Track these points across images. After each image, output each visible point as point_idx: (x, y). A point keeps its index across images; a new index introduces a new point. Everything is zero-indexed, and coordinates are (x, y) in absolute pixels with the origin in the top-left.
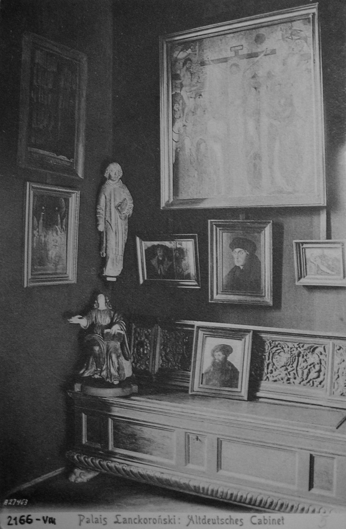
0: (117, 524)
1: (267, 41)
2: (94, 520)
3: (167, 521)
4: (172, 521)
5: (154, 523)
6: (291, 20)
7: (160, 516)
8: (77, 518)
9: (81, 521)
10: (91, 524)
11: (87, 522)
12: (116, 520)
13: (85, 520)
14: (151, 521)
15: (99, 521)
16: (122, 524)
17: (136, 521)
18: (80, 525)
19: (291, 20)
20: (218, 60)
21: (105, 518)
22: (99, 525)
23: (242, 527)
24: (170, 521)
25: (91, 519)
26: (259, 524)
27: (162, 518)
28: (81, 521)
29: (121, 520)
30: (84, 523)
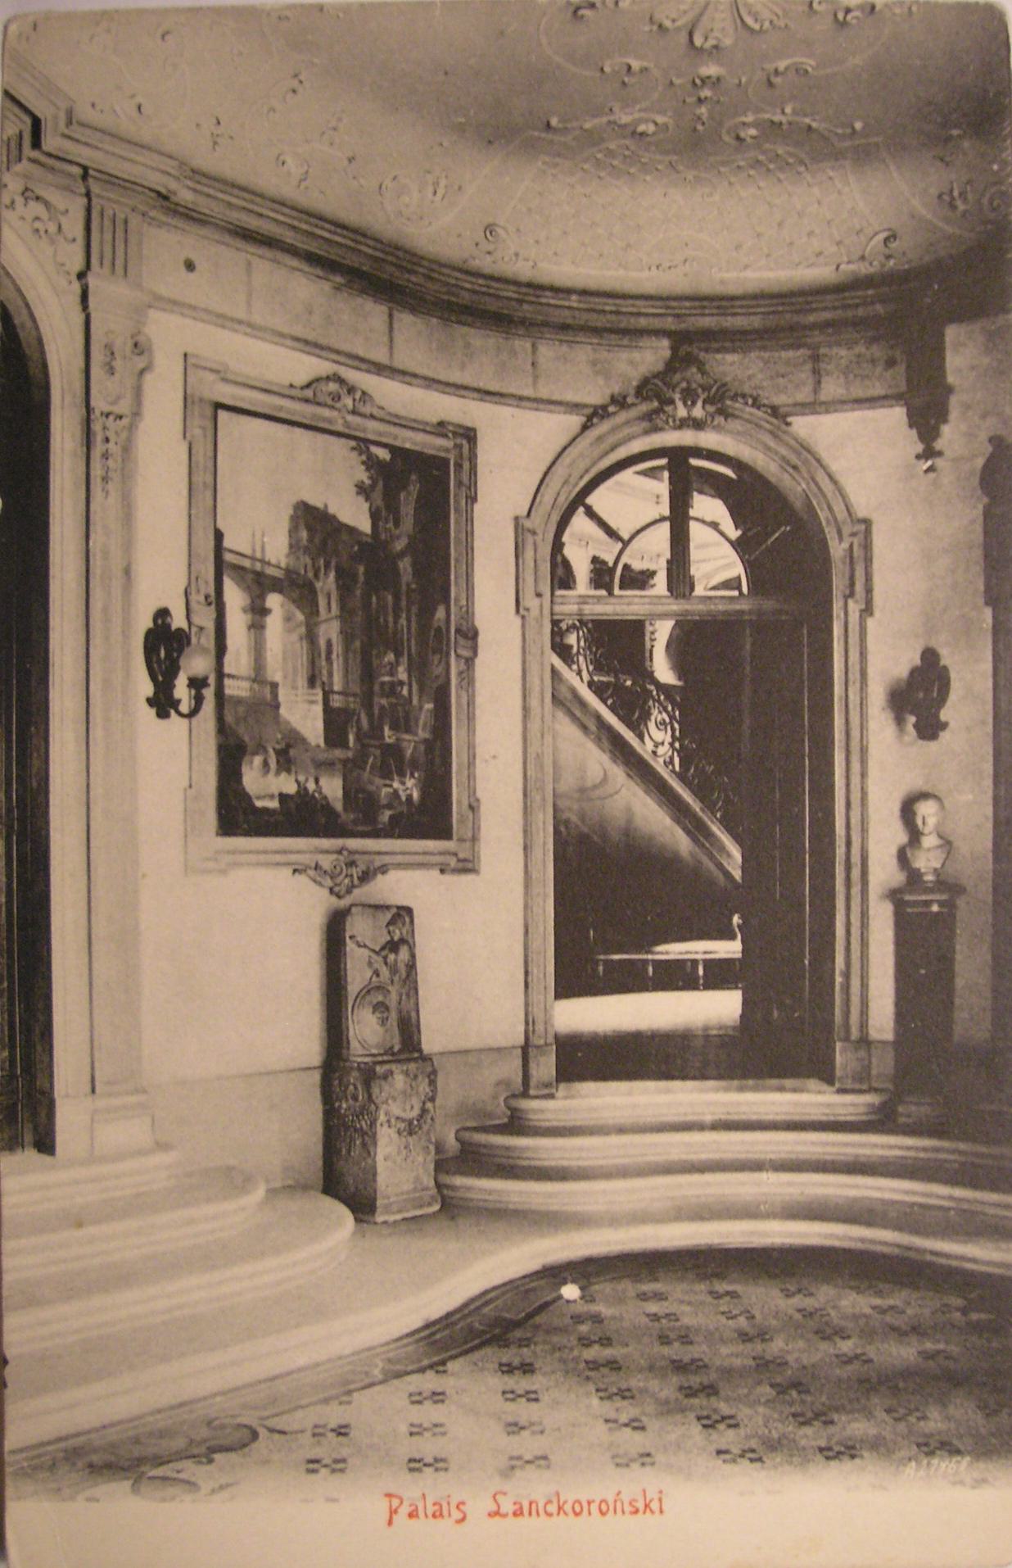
0: (497, 1518)
1: (306, 691)
2: (430, 1509)
3: (640, 1505)
4: (655, 1506)
5: (577, 1514)
6: (12, 1047)
7: (619, 1493)
8: (383, 1506)
9: (393, 1512)
10: (422, 1525)
11: (411, 1515)
12: (494, 1508)
13: (405, 1510)
14: (594, 1508)
15: (445, 1512)
16: (511, 1520)
17: (552, 1508)
18: (390, 1523)
19: (12, 1047)
20: (534, 327)
21: (463, 1503)
22: (445, 1524)
23: (464, 1524)
24: (646, 1506)
25: (420, 1506)
26: (515, 1514)
27: (626, 1498)
28: (393, 1512)
29: (507, 1506)
30: (401, 1517)
